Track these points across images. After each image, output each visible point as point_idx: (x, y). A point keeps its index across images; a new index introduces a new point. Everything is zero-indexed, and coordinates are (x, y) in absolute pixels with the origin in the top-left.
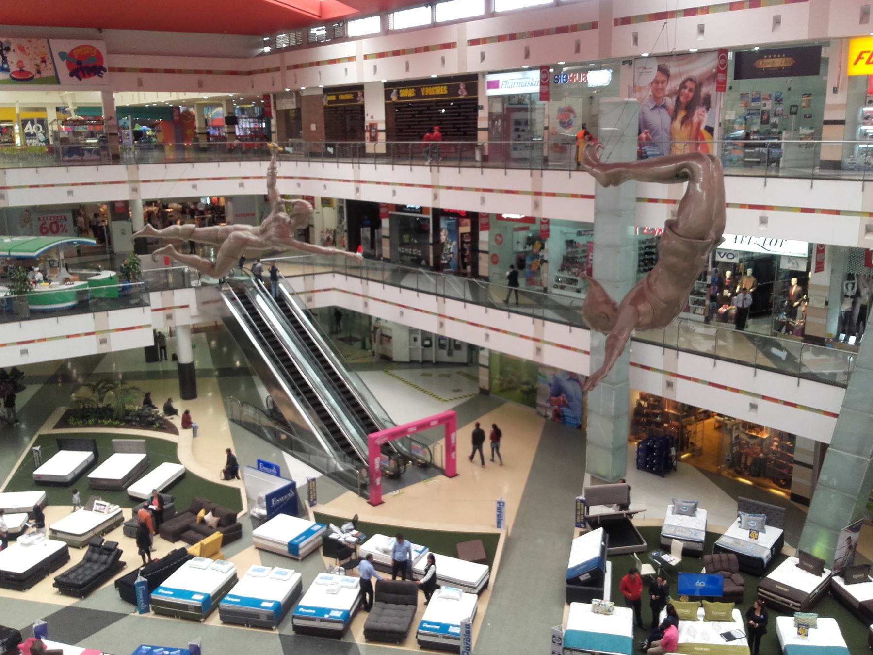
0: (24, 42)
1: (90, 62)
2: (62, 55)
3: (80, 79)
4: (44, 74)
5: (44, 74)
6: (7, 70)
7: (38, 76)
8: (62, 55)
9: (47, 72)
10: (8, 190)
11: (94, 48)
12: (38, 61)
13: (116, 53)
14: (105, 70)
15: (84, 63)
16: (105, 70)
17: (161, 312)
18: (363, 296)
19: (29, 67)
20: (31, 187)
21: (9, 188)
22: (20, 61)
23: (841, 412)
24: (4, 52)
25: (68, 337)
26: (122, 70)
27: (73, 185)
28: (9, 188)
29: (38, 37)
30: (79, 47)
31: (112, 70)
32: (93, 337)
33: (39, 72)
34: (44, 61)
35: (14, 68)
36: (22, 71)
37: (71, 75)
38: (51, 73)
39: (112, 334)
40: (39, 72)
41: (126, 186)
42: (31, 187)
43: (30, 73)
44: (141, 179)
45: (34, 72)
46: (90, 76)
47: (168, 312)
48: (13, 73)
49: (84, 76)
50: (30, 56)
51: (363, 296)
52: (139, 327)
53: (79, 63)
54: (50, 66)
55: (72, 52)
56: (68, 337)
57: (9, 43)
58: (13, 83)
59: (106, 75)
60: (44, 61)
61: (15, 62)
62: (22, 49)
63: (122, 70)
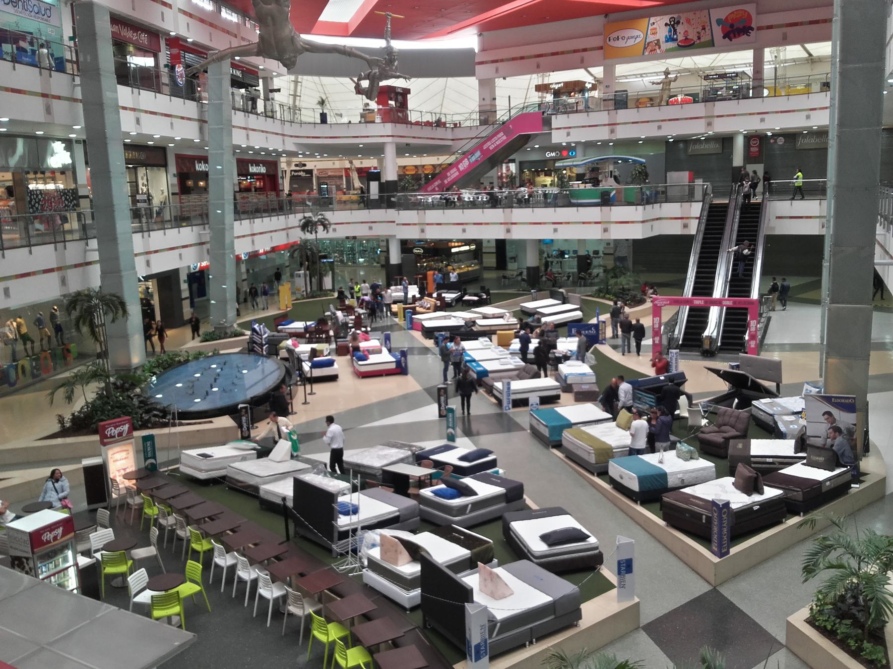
0: (690, 15)
1: (740, 25)
2: (719, 22)
3: (731, 40)
4: (702, 40)
5: (702, 40)
6: (676, 40)
7: (698, 41)
8: (719, 22)
9: (706, 38)
10: (618, 126)
11: (746, 11)
12: (700, 29)
13: (766, 13)
14: (752, 29)
15: (736, 25)
16: (752, 29)
17: (680, 220)
18: (134, 110)
19: (692, 36)
20: (633, 123)
21: (618, 124)
22: (686, 31)
23: (233, 224)
24: (675, 26)
25: (584, 223)
26: (770, 27)
27: (663, 121)
28: (618, 124)
29: (701, 9)
30: (733, 13)
31: (760, 28)
32: (599, 225)
33: (699, 38)
34: (704, 29)
35: (681, 37)
36: (686, 39)
37: (724, 37)
38: (708, 38)
39: (613, 225)
40: (699, 38)
41: (703, 120)
42: (633, 123)
43: (692, 40)
44: (716, 114)
45: (695, 38)
46: (739, 36)
47: (685, 221)
48: (680, 41)
49: (735, 37)
50: (694, 26)
51: (134, 110)
52: (633, 222)
53: (732, 26)
54: (708, 32)
55: (727, 18)
56: (584, 223)
57: (679, 17)
58: (679, 50)
59: (753, 33)
60: (704, 29)
61: (682, 33)
62: (688, 21)
63: (770, 27)
